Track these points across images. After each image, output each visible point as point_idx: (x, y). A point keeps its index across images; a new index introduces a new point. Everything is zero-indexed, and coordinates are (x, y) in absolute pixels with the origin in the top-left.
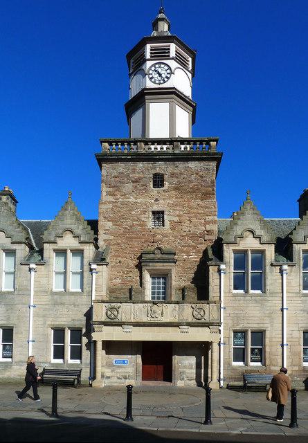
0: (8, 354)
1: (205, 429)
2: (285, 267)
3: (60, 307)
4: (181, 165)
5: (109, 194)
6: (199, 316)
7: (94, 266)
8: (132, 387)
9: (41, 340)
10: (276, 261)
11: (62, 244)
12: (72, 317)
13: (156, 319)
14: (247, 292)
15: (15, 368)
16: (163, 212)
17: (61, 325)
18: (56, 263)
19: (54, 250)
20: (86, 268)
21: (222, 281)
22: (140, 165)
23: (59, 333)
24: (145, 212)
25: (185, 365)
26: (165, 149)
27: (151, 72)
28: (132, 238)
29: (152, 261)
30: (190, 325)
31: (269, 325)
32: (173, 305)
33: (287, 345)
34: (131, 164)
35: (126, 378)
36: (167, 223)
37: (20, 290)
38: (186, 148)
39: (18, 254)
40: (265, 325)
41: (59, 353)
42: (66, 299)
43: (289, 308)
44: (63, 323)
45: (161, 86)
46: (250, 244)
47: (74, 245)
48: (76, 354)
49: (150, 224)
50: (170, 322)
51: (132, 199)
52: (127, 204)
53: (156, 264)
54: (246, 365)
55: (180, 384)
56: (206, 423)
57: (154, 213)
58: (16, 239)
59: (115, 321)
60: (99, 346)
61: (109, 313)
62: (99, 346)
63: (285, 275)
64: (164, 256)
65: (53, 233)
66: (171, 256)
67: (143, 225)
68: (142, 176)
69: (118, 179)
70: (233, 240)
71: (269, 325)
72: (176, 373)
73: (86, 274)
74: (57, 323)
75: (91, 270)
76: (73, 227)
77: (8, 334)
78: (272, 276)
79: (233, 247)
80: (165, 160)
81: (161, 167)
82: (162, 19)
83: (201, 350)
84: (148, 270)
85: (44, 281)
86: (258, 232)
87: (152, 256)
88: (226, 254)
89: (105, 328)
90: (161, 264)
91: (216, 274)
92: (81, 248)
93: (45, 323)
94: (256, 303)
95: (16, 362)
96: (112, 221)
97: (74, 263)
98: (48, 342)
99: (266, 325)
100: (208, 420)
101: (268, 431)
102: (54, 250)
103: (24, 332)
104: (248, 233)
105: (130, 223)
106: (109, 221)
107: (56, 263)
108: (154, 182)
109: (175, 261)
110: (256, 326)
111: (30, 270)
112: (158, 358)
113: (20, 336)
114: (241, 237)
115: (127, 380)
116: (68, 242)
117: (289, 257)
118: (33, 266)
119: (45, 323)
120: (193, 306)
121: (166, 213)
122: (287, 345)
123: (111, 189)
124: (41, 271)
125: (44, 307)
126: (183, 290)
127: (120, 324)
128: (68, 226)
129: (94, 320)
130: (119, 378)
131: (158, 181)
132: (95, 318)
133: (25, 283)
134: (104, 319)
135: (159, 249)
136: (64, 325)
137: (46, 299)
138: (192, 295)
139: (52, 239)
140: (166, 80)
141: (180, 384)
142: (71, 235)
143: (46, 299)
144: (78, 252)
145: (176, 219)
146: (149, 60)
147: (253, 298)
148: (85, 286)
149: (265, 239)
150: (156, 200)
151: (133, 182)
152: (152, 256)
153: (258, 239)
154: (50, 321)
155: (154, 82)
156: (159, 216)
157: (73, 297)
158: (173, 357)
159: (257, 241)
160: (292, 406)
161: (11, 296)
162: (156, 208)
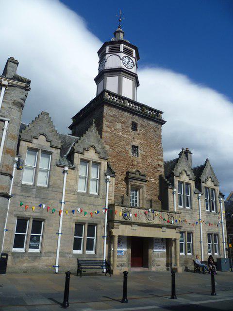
0: (34, 244)
2: (67, 169)
4: (146, 121)
5: (107, 126)
8: (128, 273)
9: (67, 233)
10: (60, 162)
11: (35, 144)
13: (150, 222)
15: (43, 258)
16: (137, 147)
17: (84, 220)
20: (102, 177)
22: (126, 114)
24: (128, 145)
25: (157, 254)
26: (115, 100)
28: (121, 160)
29: (135, 179)
34: (120, 111)
35: (122, 266)
36: (140, 155)
37: (53, 187)
38: (113, 99)
42: (88, 199)
45: (128, 70)
46: (185, 178)
49: (131, 154)
50: (141, 222)
51: (120, 134)
52: (118, 136)
53: (137, 181)
55: (153, 269)
56: (212, 294)
57: (133, 146)
59: (127, 221)
60: (116, 239)
64: (141, 177)
65: (82, 146)
66: (144, 178)
67: (127, 153)
68: (126, 121)
69: (112, 118)
71: (194, 229)
72: (150, 262)
73: (102, 182)
75: (106, 180)
76: (95, 145)
80: (139, 116)
81: (136, 119)
82: (120, 31)
83: (168, 243)
85: (73, 183)
87: (134, 175)
89: (122, 227)
90: (139, 182)
91: (171, 194)
92: (100, 162)
93: (71, 218)
94: (189, 215)
95: (45, 253)
96: (109, 145)
97: (94, 173)
100: (213, 292)
103: (54, 225)
104: (184, 172)
105: (120, 150)
106: (107, 144)
107: (82, 170)
108: (132, 126)
109: (145, 181)
110: (189, 229)
111: (64, 172)
112: (140, 249)
113: (51, 228)
115: (123, 268)
116: (91, 155)
117: (200, 190)
118: (67, 169)
121: (139, 148)
123: (109, 124)
124: (71, 174)
125: (72, 204)
126: (151, 201)
127: (131, 224)
128: (92, 144)
129: (115, 219)
131: (134, 127)
132: (116, 218)
133: (59, 182)
135: (138, 171)
136: (86, 221)
137: (73, 198)
138: (158, 206)
139: (80, 151)
141: (153, 269)
142: (185, 174)
144: (96, 164)
145: (144, 153)
147: (187, 212)
148: (101, 191)
150: (134, 138)
151: (121, 123)
152: (134, 175)
154: (75, 217)
155: (125, 66)
156: (135, 148)
158: (149, 250)
160: (174, 280)
161: (45, 192)
162: (134, 144)
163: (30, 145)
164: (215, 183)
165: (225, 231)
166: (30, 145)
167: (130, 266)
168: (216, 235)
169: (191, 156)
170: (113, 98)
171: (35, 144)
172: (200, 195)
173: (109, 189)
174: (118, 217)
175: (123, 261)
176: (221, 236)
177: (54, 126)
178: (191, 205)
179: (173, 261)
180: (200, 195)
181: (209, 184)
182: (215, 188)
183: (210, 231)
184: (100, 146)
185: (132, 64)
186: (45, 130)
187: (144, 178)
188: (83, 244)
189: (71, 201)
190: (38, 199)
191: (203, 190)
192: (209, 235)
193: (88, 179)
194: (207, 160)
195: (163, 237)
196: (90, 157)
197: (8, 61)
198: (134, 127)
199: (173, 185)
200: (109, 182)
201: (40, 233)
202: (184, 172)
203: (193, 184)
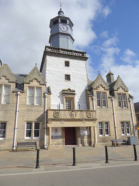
1: (107, 166)
2: (19, 93)
3: (30, 112)
6: (89, 117)
7: (46, 95)
11: (32, 84)
12: (33, 117)
14: (102, 107)
18: (28, 92)
19: (29, 86)
21: (94, 103)
23: (29, 124)
26: (49, 50)
27: (61, 27)
30: (86, 120)
31: (110, 120)
32: (80, 112)
33: (17, 128)
35: (59, 145)
38: (80, 55)
39: (12, 87)
40: (109, 120)
41: (29, 134)
42: (33, 108)
43: (20, 111)
44: (32, 119)
46: (101, 89)
47: (38, 85)
48: (37, 135)
54: (104, 136)
58: (106, 88)
61: (57, 115)
62: (51, 129)
63: (113, 101)
66: (73, 93)
70: (28, 82)
74: (29, 119)
76: (37, 78)
77: (4, 125)
78: (109, 101)
79: (96, 90)
84: (65, 97)
86: (104, 86)
88: (25, 88)
91: (92, 101)
93: (23, 120)
95: (7, 140)
98: (24, 128)
99: (109, 120)
101: (82, 168)
102: (29, 86)
104: (101, 86)
110: (106, 120)
114: (32, 81)
115: (59, 145)
117: (113, 95)
119: (23, 120)
120: (87, 112)
122: (17, 128)
130: (56, 145)
131: (67, 64)
132: (49, 117)
134: (53, 117)
140: (66, 31)
142: (101, 87)
143: (25, 108)
146: (60, 23)
149: (106, 88)
153: (39, 83)
154: (26, 119)
157: (37, 108)
159: (103, 89)
163: (29, 85)
164: (125, 90)
165: (135, 119)
166: (29, 85)
167: (64, 144)
168: (128, 123)
169: (113, 76)
170: (79, 54)
171: (32, 84)
172: (113, 98)
173: (47, 101)
174: (51, 116)
175: (59, 142)
176: (131, 122)
177: (10, 69)
178: (107, 105)
179: (93, 140)
180: (113, 98)
181: (121, 91)
182: (125, 93)
183: (122, 120)
184: (40, 78)
185: (67, 28)
186: (6, 73)
187: (73, 93)
188: (104, 132)
189: (25, 110)
190: (2, 111)
191: (116, 95)
192: (122, 123)
193: (32, 97)
194: (119, 76)
195: (57, 126)
196: (34, 85)
197: (46, 53)
198: (67, 64)
199: (93, 94)
200: (47, 97)
201: (26, 130)
202: (100, 86)
203: (108, 92)
